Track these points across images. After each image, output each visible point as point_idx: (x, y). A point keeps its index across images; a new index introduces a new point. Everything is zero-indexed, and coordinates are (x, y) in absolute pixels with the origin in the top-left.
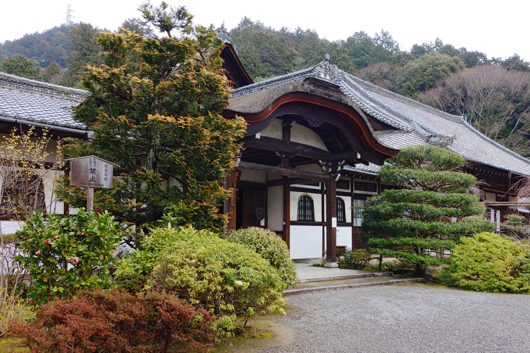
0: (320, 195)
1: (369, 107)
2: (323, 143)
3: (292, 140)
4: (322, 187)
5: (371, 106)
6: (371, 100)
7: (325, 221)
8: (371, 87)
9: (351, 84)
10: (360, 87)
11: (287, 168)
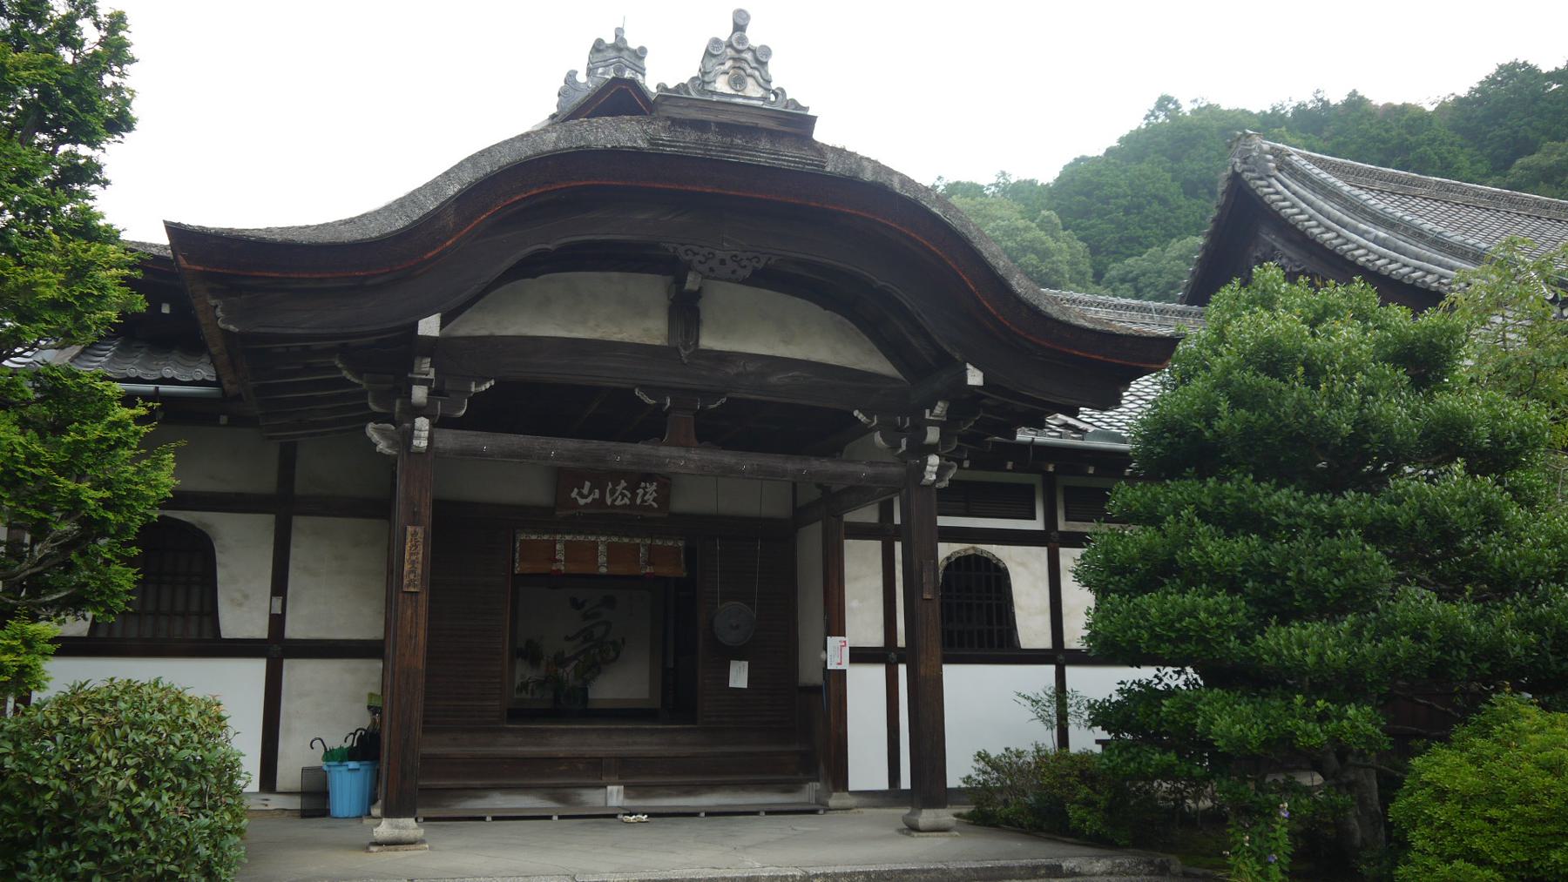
0: (875, 546)
1: (1363, 241)
2: (870, 344)
3: (708, 342)
4: (1050, 520)
5: (1376, 240)
6: (1379, 219)
7: (901, 642)
8: (1411, 182)
9: (1312, 181)
10: (1339, 183)
11: (687, 446)
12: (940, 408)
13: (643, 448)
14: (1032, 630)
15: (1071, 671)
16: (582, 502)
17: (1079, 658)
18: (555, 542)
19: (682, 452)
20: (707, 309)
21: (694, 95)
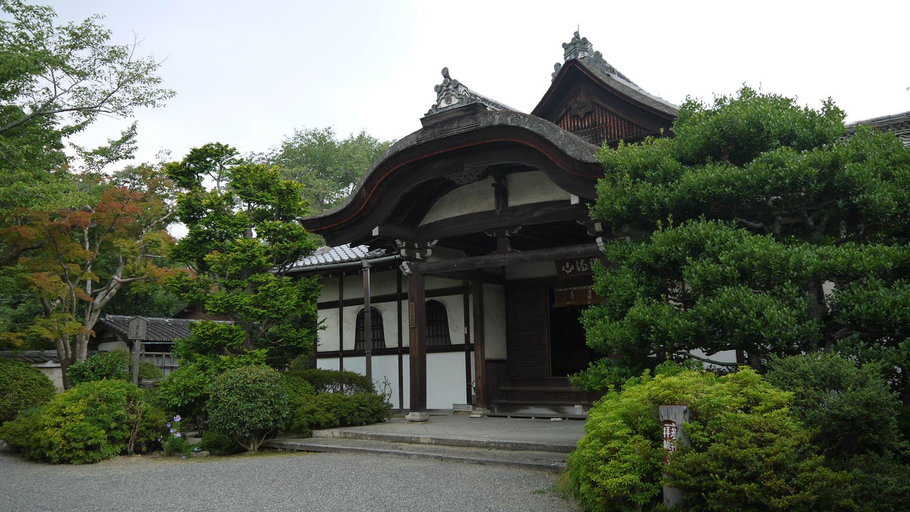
3: (512, 203)
12: (435, 242)
13: (488, 257)
14: (391, 341)
15: (345, 360)
16: (568, 272)
17: (350, 354)
18: (569, 292)
19: (503, 256)
20: (511, 188)
21: (435, 112)
